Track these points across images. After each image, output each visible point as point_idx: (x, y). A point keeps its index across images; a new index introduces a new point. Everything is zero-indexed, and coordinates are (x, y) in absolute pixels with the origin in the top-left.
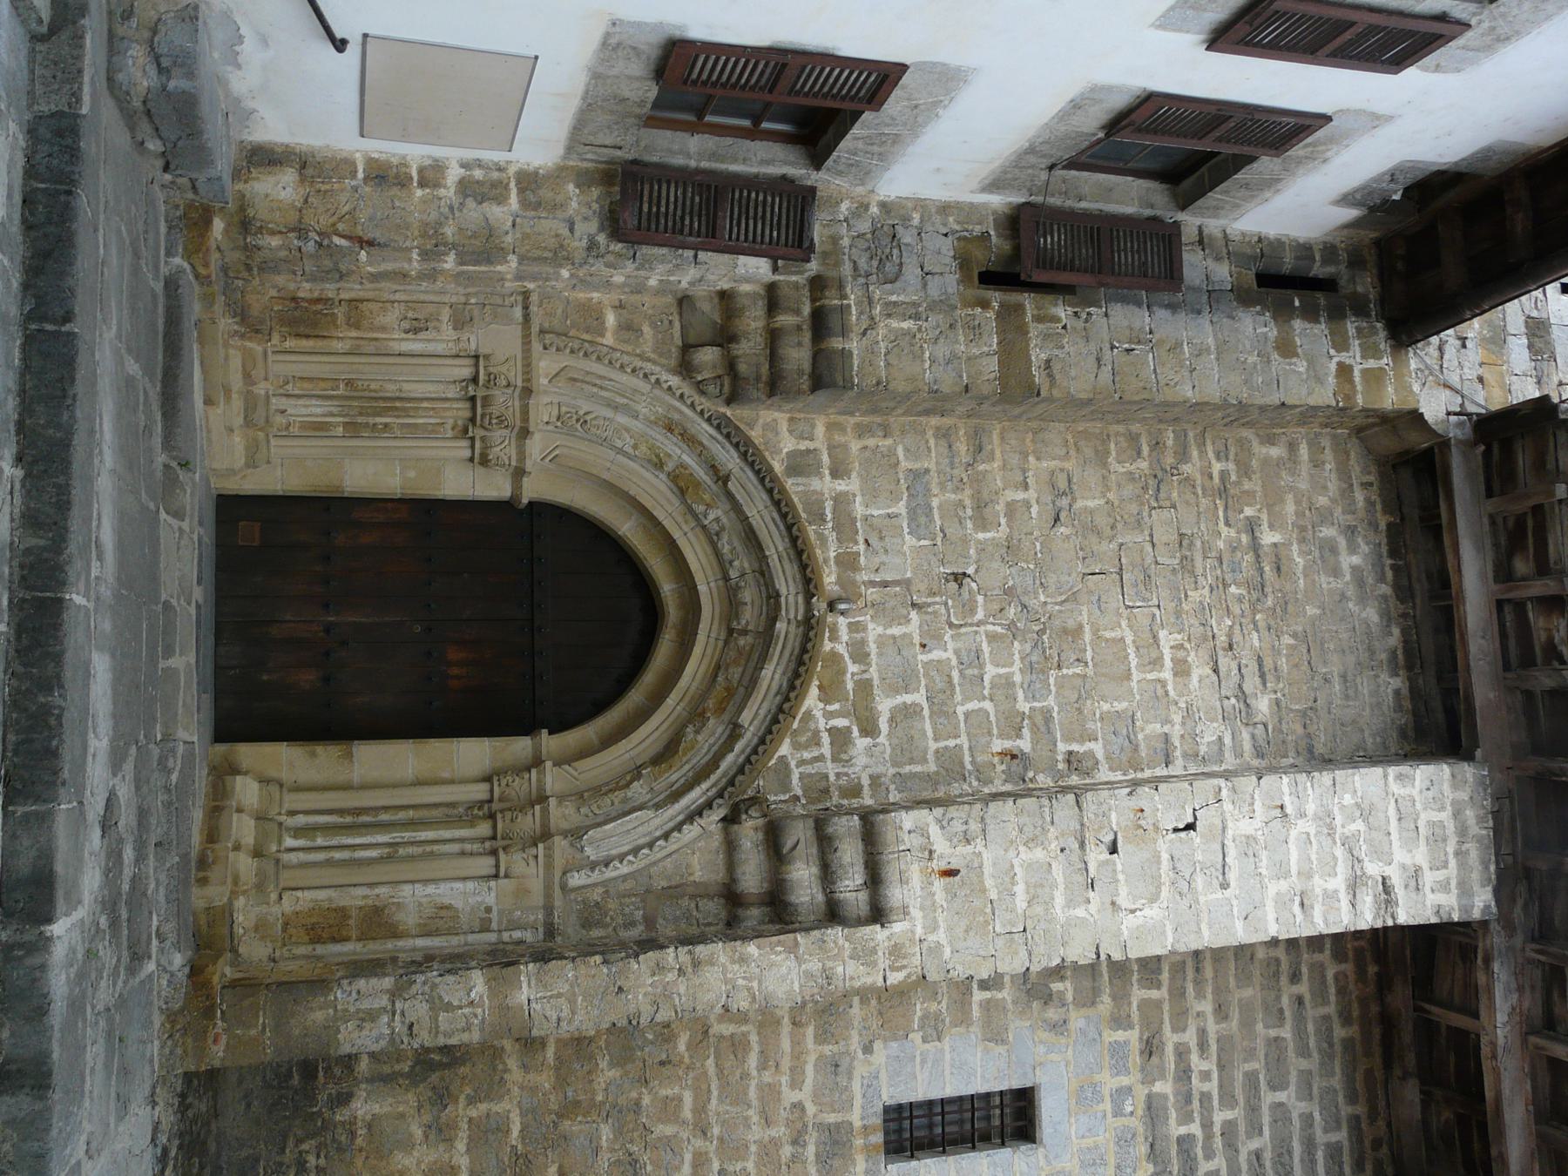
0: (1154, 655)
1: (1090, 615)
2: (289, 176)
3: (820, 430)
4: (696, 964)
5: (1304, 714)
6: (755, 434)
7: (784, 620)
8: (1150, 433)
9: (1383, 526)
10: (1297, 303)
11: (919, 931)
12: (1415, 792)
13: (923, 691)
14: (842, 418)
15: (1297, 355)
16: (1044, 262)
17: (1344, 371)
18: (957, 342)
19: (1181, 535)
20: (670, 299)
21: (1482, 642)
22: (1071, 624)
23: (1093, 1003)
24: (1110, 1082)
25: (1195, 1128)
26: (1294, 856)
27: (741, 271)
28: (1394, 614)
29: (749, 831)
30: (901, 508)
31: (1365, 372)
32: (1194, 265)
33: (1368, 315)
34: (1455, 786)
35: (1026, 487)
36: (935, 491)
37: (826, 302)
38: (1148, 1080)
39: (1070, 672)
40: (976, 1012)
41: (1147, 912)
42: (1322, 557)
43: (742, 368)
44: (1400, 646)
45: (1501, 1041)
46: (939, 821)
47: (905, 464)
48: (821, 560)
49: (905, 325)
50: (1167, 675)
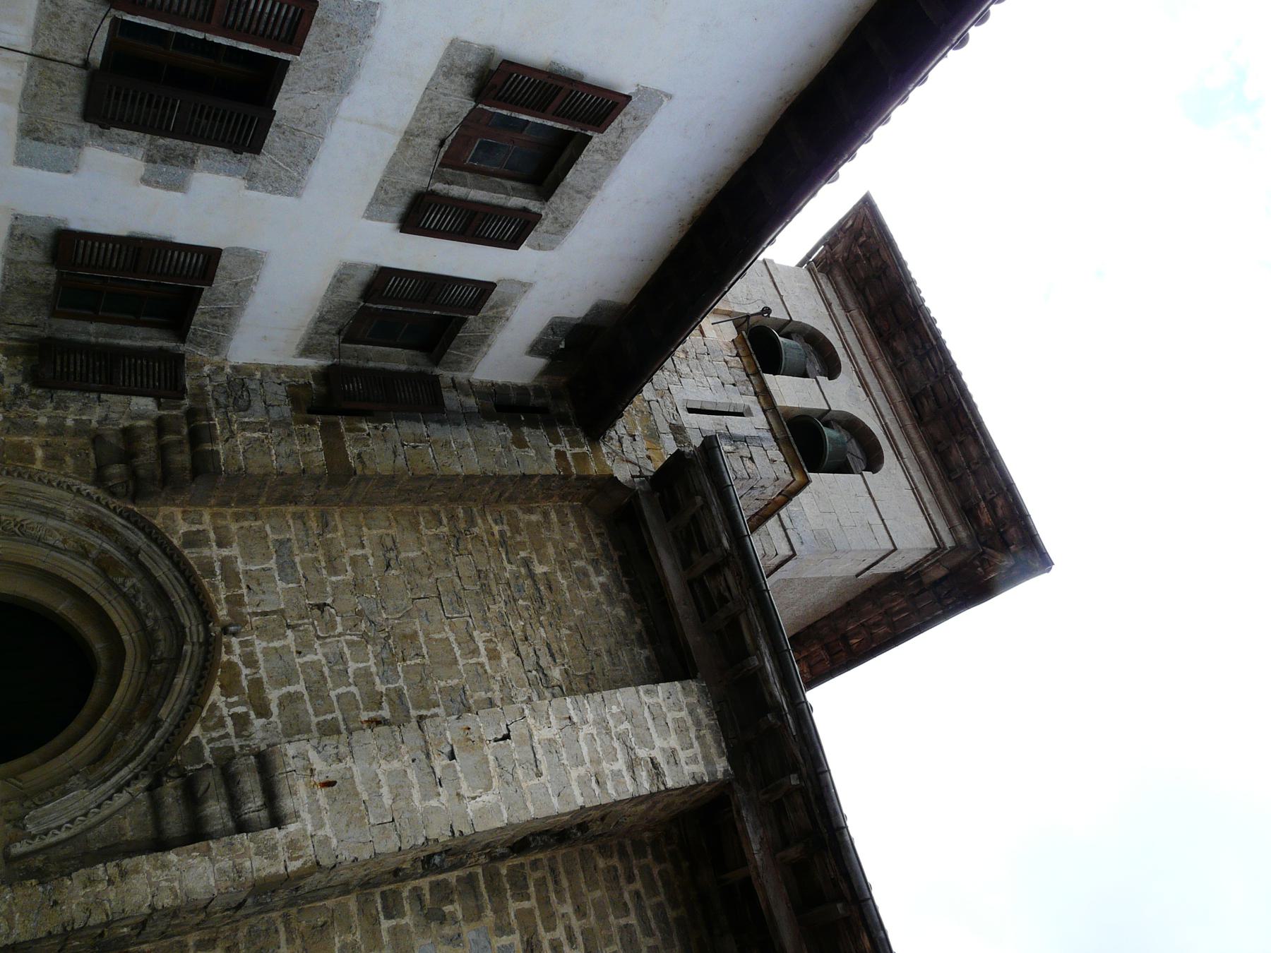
3: (207, 518)
4: (124, 874)
6: (158, 522)
7: (187, 633)
11: (310, 828)
12: (660, 700)
13: (302, 683)
14: (223, 510)
17: (560, 455)
19: (479, 571)
20: (84, 440)
22: (408, 631)
23: (479, 918)
26: (585, 750)
27: (134, 408)
29: (170, 791)
30: (272, 564)
31: (574, 455)
32: (451, 399)
35: (363, 547)
40: (385, 937)
41: (484, 797)
43: (142, 472)
45: (759, 863)
46: (315, 748)
47: (272, 536)
49: (256, 435)
50: (483, 659)
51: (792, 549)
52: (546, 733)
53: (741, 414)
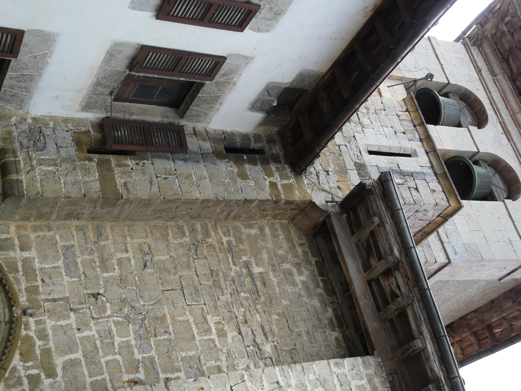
0: (206, 327)
1: (169, 310)
3: (13, 229)
5: (290, 351)
8: (188, 225)
9: (313, 262)
10: (245, 158)
12: (346, 371)
13: (80, 352)
14: (24, 223)
15: (249, 179)
16: (118, 141)
17: (273, 185)
18: (77, 175)
19: (212, 271)
21: (365, 300)
22: (159, 314)
28: (327, 302)
30: (60, 263)
31: (283, 186)
32: (192, 143)
33: (280, 162)
34: (366, 367)
35: (127, 251)
36: (78, 254)
37: (7, 159)
39: (162, 338)
42: (285, 278)
44: (333, 317)
47: (60, 243)
48: (17, 290)
49: (50, 168)
50: (214, 336)
51: (448, 258)
53: (409, 156)
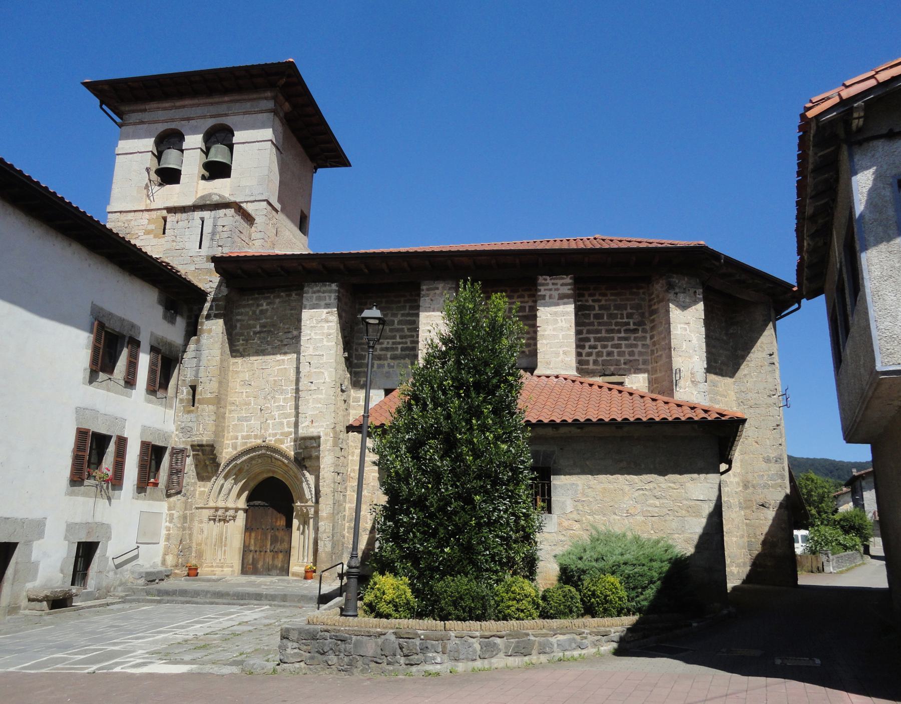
2: (167, 557)
6: (228, 457)
7: (264, 453)
24: (386, 369)
25: (400, 346)
30: (245, 423)
38: (386, 359)
52: (311, 349)
53: (203, 222)
